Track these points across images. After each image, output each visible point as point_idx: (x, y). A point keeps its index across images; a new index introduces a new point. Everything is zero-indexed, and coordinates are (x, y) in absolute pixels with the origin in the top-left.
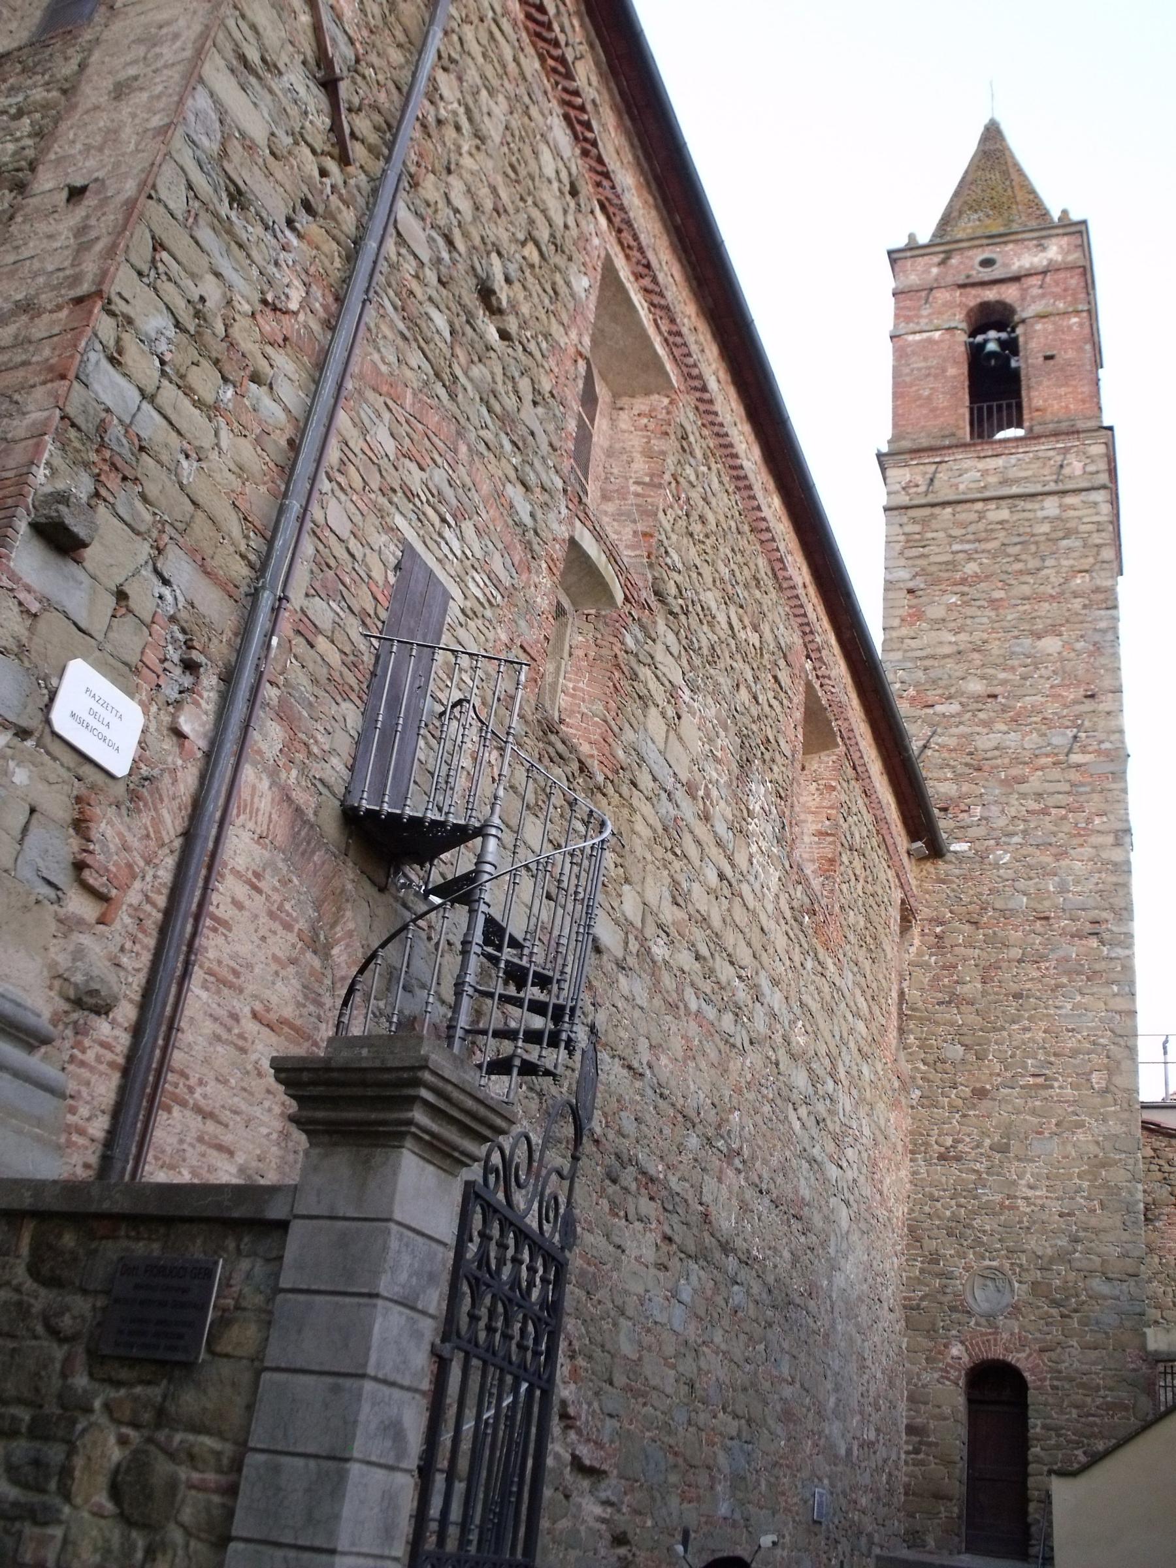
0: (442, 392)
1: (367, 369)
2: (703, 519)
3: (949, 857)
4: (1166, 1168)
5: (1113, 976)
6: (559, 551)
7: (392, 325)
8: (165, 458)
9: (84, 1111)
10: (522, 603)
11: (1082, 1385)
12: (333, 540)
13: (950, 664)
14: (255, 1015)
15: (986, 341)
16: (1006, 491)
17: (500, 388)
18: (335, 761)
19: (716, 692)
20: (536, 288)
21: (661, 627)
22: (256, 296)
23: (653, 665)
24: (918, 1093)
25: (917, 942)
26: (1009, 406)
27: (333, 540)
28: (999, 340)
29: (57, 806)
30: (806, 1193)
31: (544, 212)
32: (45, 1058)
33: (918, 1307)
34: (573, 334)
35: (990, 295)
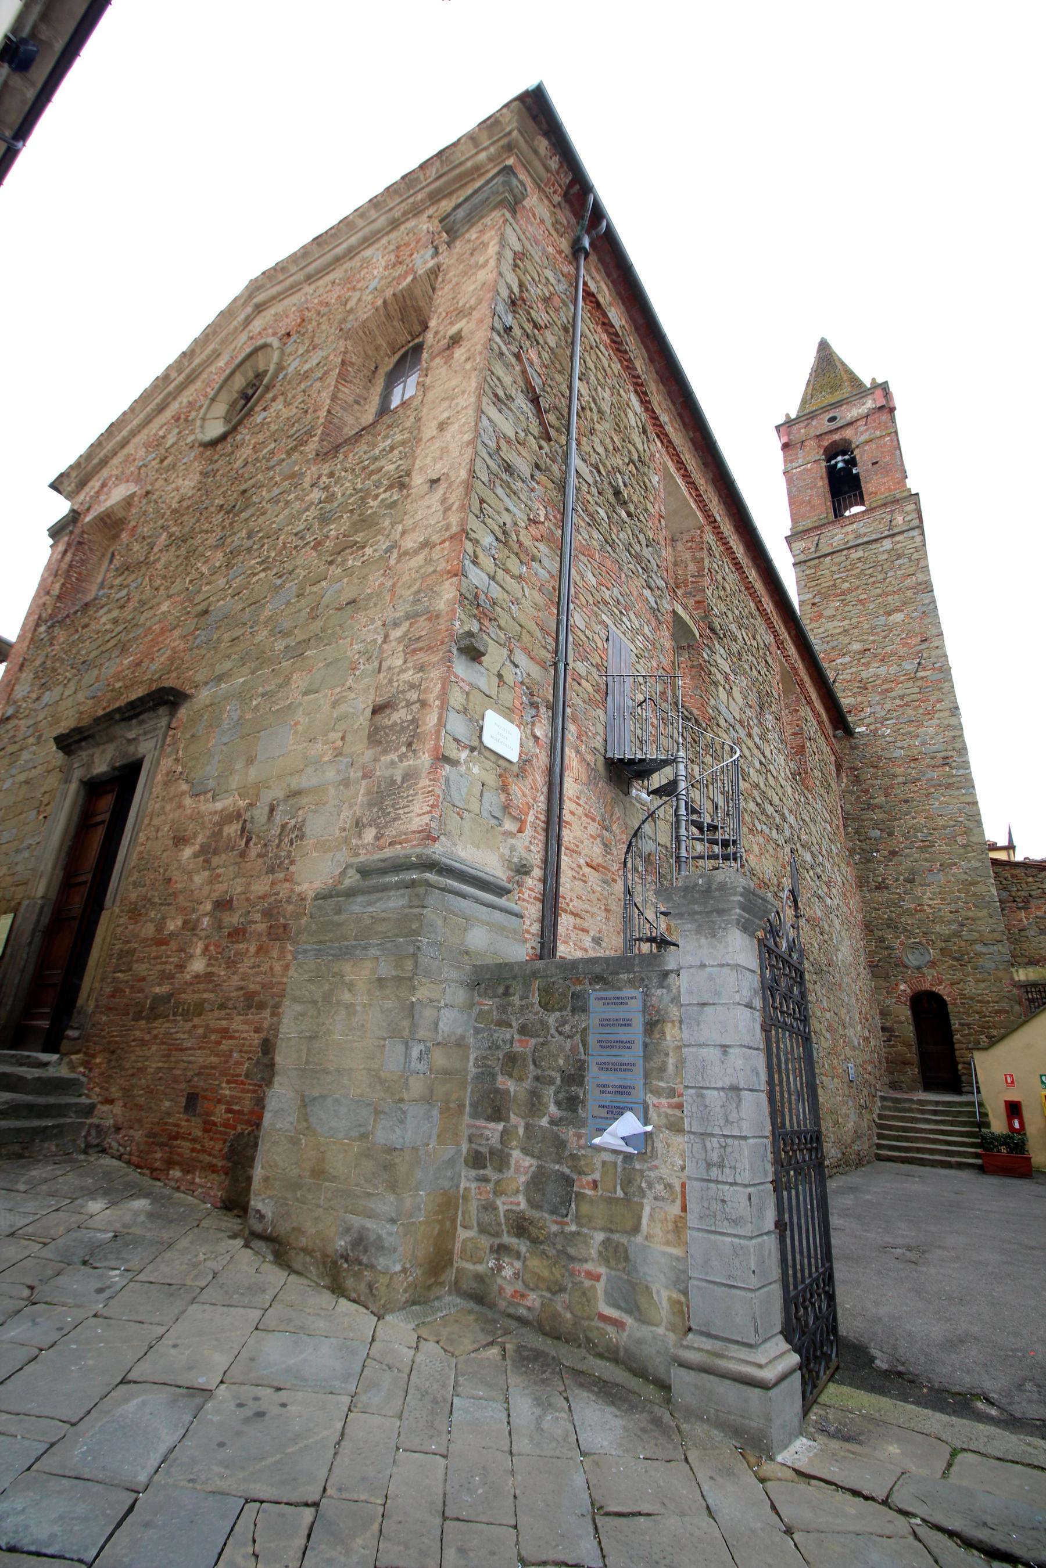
0: (609, 549)
1: (578, 544)
2: (724, 588)
3: (856, 735)
4: (1004, 882)
5: (960, 785)
6: (669, 618)
7: (583, 520)
8: (504, 606)
9: (528, 922)
10: (658, 646)
11: (979, 1002)
12: (579, 633)
13: (841, 638)
14: (587, 864)
15: (837, 463)
16: (860, 541)
17: (632, 541)
18: (598, 738)
19: (745, 673)
20: (637, 487)
21: (717, 646)
22: (526, 518)
23: (717, 666)
24: (858, 856)
25: (845, 780)
26: (855, 495)
27: (579, 633)
28: (844, 461)
29: (491, 779)
30: (819, 913)
31: (634, 445)
32: (508, 900)
33: (877, 966)
34: (657, 507)
35: (836, 437)
